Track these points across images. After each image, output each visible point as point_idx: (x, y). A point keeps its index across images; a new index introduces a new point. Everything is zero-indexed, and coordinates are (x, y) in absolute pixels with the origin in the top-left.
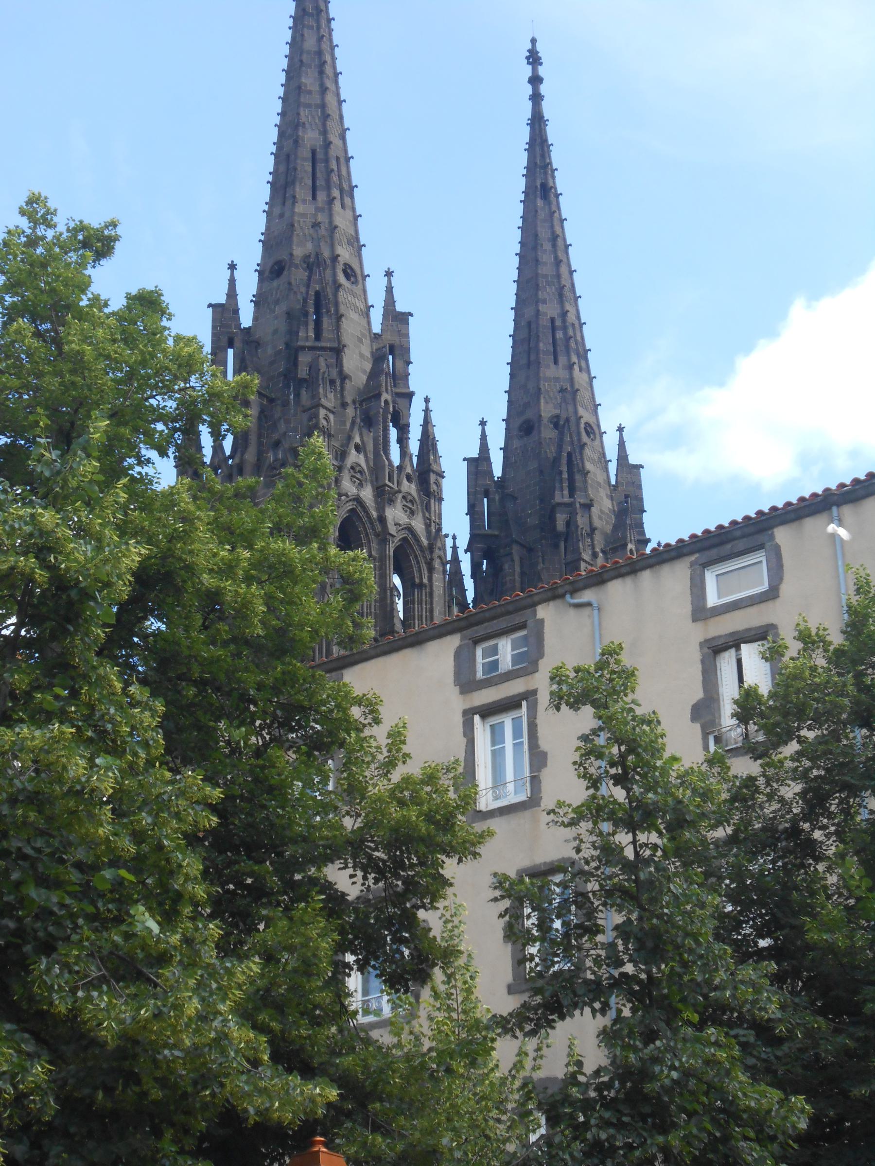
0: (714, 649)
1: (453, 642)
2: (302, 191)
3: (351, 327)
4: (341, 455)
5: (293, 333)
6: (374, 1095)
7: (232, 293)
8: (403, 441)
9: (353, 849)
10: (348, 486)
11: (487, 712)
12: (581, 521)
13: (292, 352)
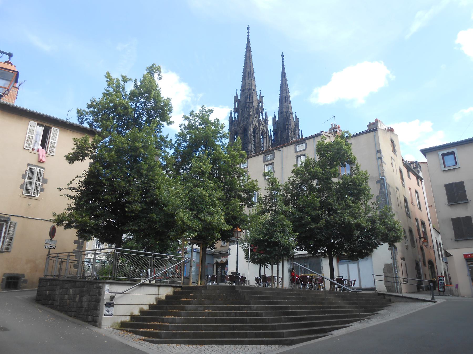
0: (298, 157)
1: (263, 155)
2: (247, 78)
3: (254, 99)
4: (253, 118)
5: (246, 100)
6: (245, 221)
7: (237, 94)
8: (262, 116)
9: (244, 190)
10: (254, 123)
11: (267, 165)
12: (289, 127)
13: (246, 103)
